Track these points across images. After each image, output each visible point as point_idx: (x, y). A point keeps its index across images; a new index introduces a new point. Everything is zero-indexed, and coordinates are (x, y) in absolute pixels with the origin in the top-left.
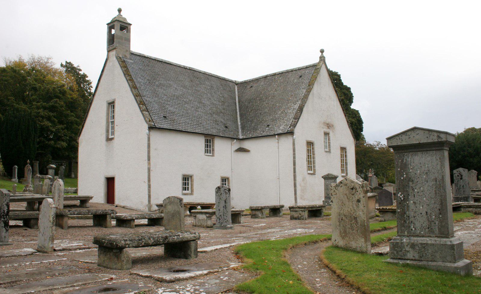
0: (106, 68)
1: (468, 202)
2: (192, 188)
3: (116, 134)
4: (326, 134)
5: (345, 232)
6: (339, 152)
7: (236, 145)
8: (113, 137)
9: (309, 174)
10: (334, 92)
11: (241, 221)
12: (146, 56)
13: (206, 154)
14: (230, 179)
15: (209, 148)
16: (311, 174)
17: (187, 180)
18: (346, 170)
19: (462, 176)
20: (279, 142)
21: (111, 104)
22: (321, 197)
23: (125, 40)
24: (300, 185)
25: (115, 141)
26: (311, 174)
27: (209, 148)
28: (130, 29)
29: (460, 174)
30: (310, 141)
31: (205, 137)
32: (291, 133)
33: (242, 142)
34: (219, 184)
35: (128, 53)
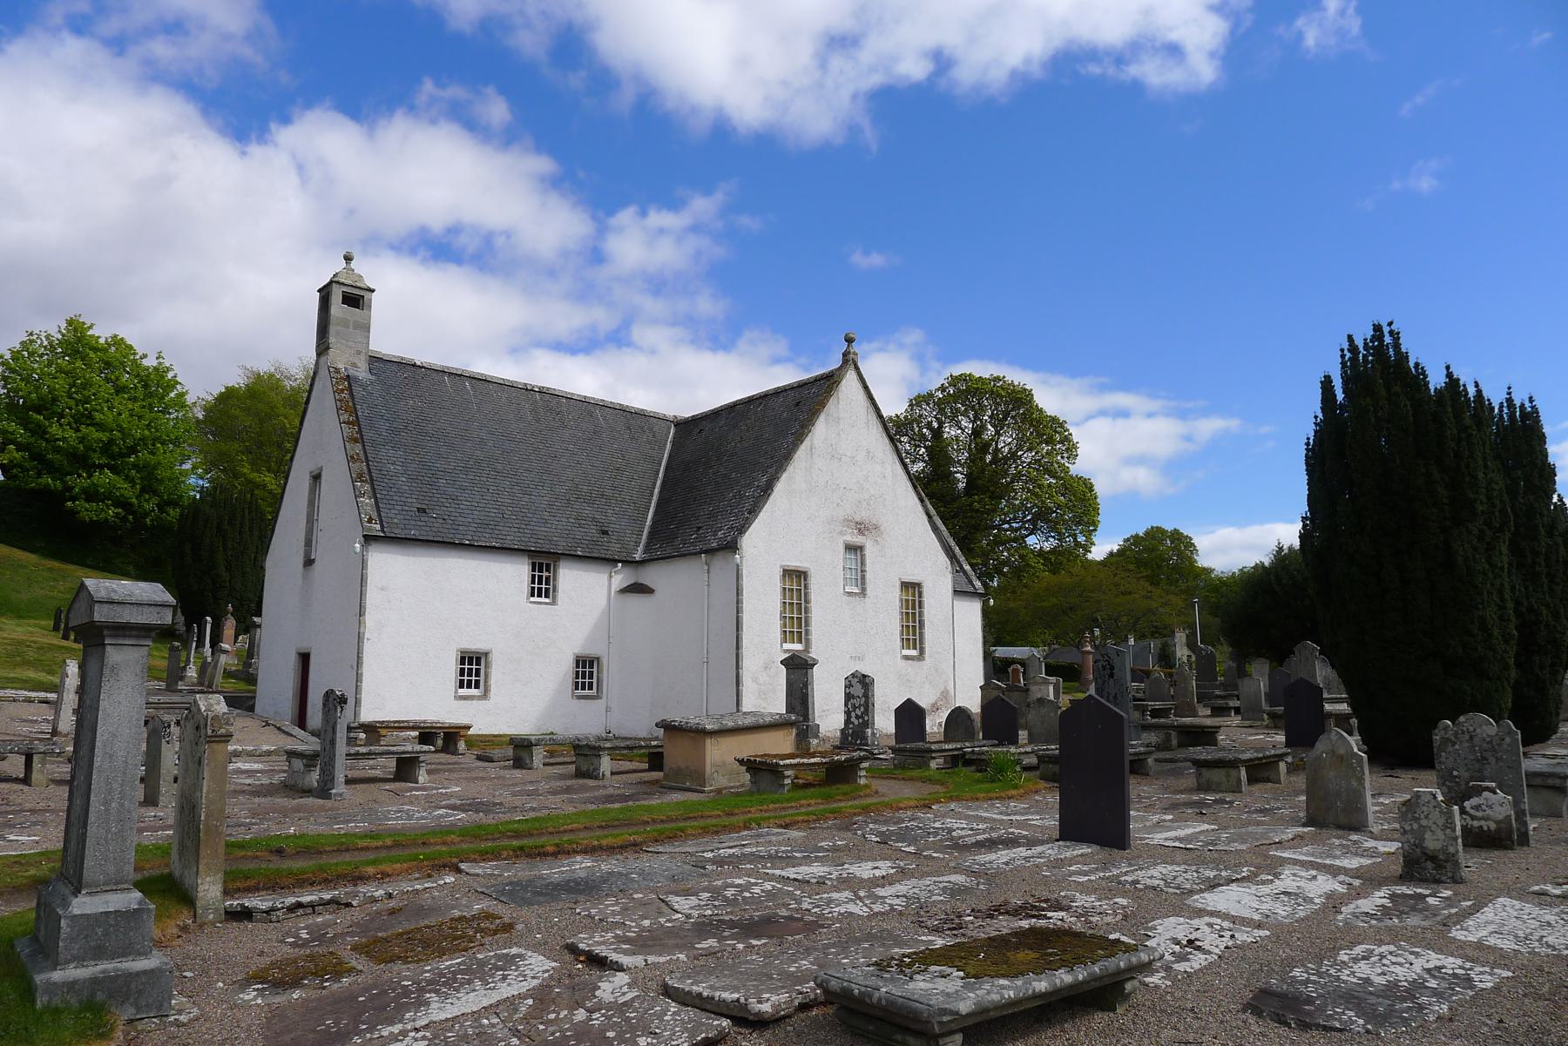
2: (486, 682)
4: (854, 549)
6: (895, 594)
7: (620, 578)
9: (907, 658)
10: (887, 441)
11: (420, 778)
12: (418, 363)
14: (604, 661)
15: (542, 587)
17: (472, 667)
18: (921, 642)
19: (1112, 668)
20: (711, 570)
21: (316, 478)
22: (828, 710)
23: (355, 328)
24: (755, 680)
25: (317, 566)
27: (542, 587)
28: (370, 300)
29: (1109, 664)
30: (797, 567)
31: (529, 557)
32: (732, 547)
35: (363, 357)
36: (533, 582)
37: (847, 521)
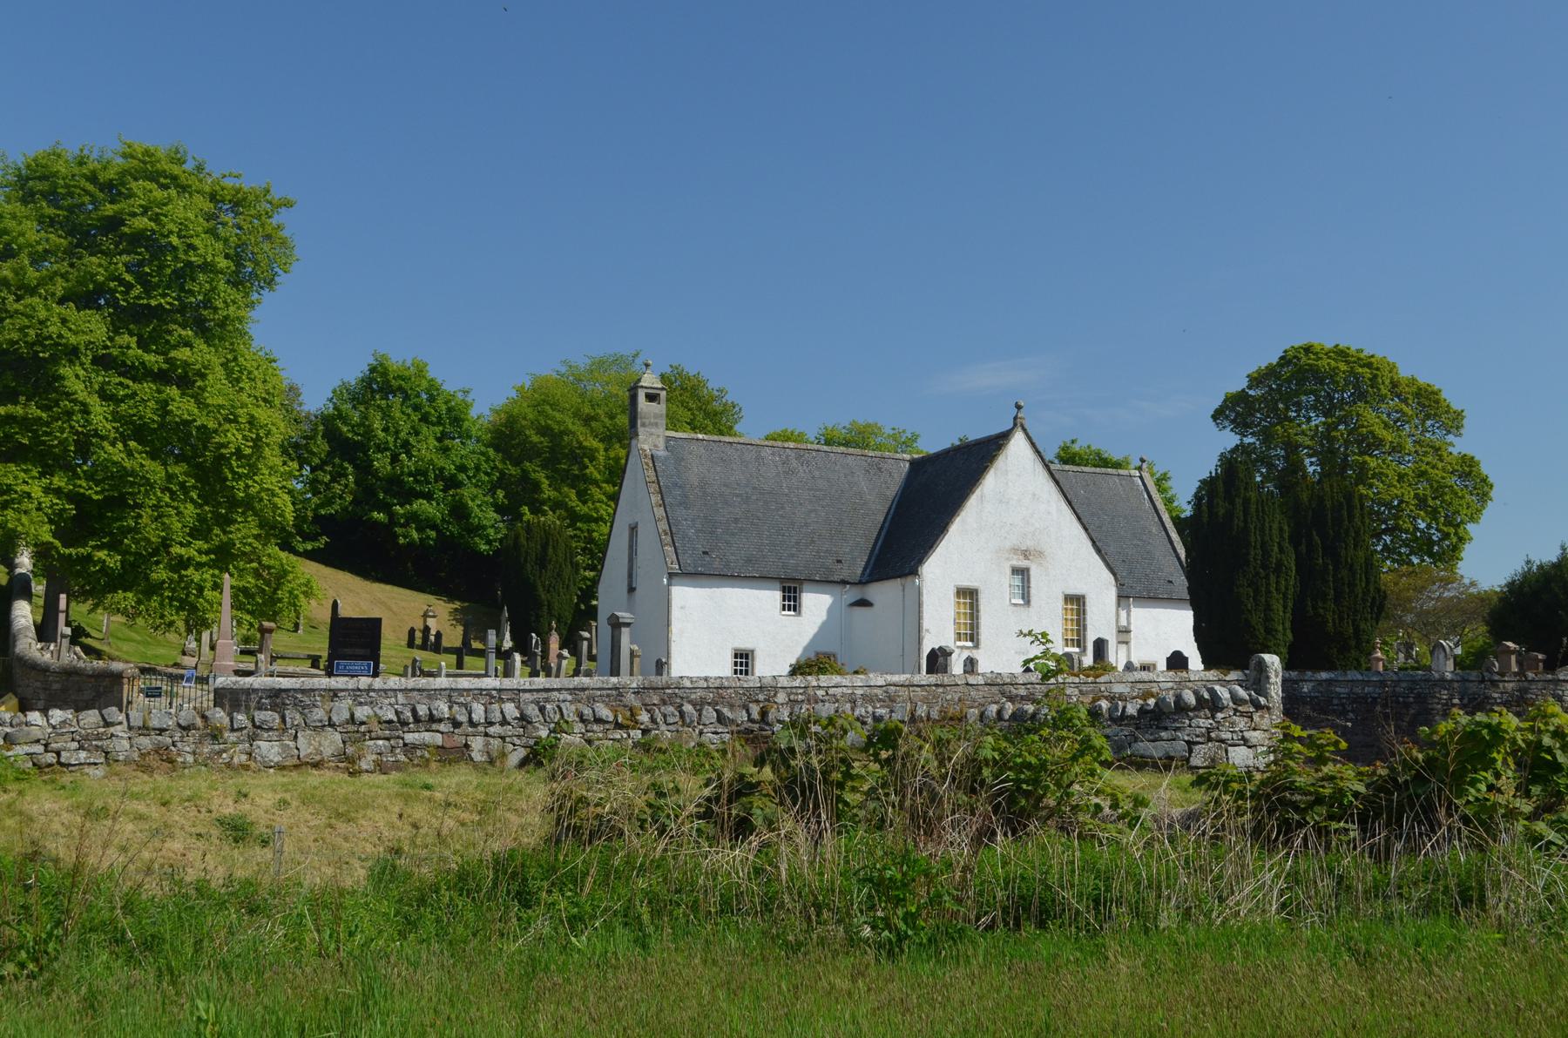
21: (633, 529)
36: (784, 600)
37: (1015, 550)
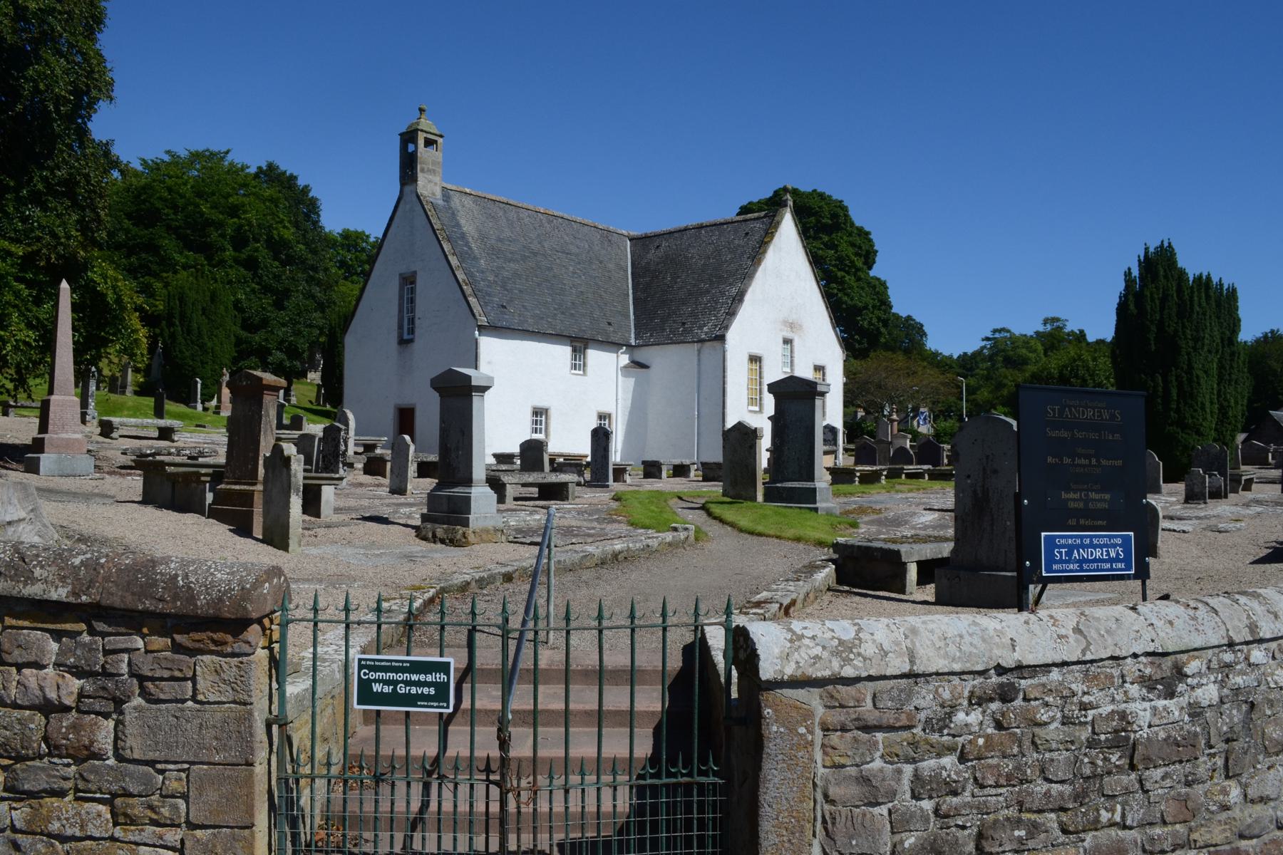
0: (398, 214)
1: (139, 421)
3: (417, 331)
4: (787, 341)
5: (831, 515)
8: (411, 337)
9: (751, 411)
13: (573, 371)
16: (755, 412)
21: (408, 281)
25: (417, 345)
26: (755, 412)
33: (635, 349)
34: (594, 424)
